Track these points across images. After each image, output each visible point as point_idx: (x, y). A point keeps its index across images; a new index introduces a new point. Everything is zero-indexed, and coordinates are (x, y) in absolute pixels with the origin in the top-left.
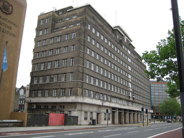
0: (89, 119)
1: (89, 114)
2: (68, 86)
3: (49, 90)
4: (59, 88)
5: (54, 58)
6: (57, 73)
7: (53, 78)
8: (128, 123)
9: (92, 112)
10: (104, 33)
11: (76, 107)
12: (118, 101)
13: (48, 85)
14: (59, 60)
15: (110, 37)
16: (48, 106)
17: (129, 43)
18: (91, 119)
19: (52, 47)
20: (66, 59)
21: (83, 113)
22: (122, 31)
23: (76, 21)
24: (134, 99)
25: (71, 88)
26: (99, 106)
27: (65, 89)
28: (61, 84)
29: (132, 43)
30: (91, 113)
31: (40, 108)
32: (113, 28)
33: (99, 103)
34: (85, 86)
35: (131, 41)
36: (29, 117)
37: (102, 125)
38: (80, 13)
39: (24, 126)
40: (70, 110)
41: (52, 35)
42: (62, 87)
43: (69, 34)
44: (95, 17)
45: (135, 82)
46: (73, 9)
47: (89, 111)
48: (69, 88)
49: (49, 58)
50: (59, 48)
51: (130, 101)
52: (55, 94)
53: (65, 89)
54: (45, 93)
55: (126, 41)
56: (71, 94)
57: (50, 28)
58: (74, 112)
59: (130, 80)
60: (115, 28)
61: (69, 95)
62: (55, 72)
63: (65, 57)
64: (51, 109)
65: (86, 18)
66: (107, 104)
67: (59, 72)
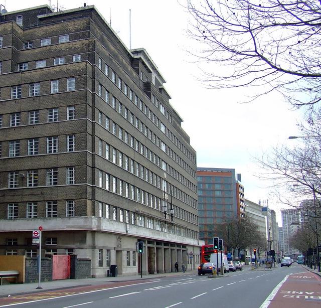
0: (105, 263)
1: (105, 252)
2: (62, 196)
3: (16, 203)
4: (21, 201)
5: (24, 134)
6: (36, 168)
7: (23, 179)
8: (147, 274)
9: (109, 250)
10: (123, 74)
11: (86, 241)
12: (155, 225)
13: (12, 193)
14: (37, 139)
15: (131, 81)
16: (16, 240)
17: (160, 87)
18: (108, 263)
19: (17, 108)
20: (55, 137)
21: (97, 251)
22: (149, 60)
23: (70, 48)
24: (172, 217)
25: (70, 201)
26: (120, 236)
27: (36, 204)
28: (45, 191)
29: (165, 86)
30: (108, 251)
31: (16, 244)
32: (131, 54)
33: (120, 229)
34: (99, 196)
35: (164, 82)
36: (28, 265)
37: (124, 276)
38: (77, 30)
39: (22, 283)
40: (71, 246)
41: (16, 79)
42: (48, 198)
43: (58, 79)
44: (105, 38)
45: (128, 172)
46: (51, 15)
47: (105, 247)
48: (67, 200)
49: (12, 131)
50: (35, 110)
51: (165, 222)
52: (32, 212)
53: (36, 204)
54: (6, 211)
55: (154, 83)
56: (70, 212)
57: (10, 63)
58: (80, 250)
59: (165, 176)
60: (136, 57)
61: (47, 215)
62: (28, 164)
63: (53, 132)
64: (24, 245)
65: (94, 45)
66: (133, 231)
67: (38, 164)
